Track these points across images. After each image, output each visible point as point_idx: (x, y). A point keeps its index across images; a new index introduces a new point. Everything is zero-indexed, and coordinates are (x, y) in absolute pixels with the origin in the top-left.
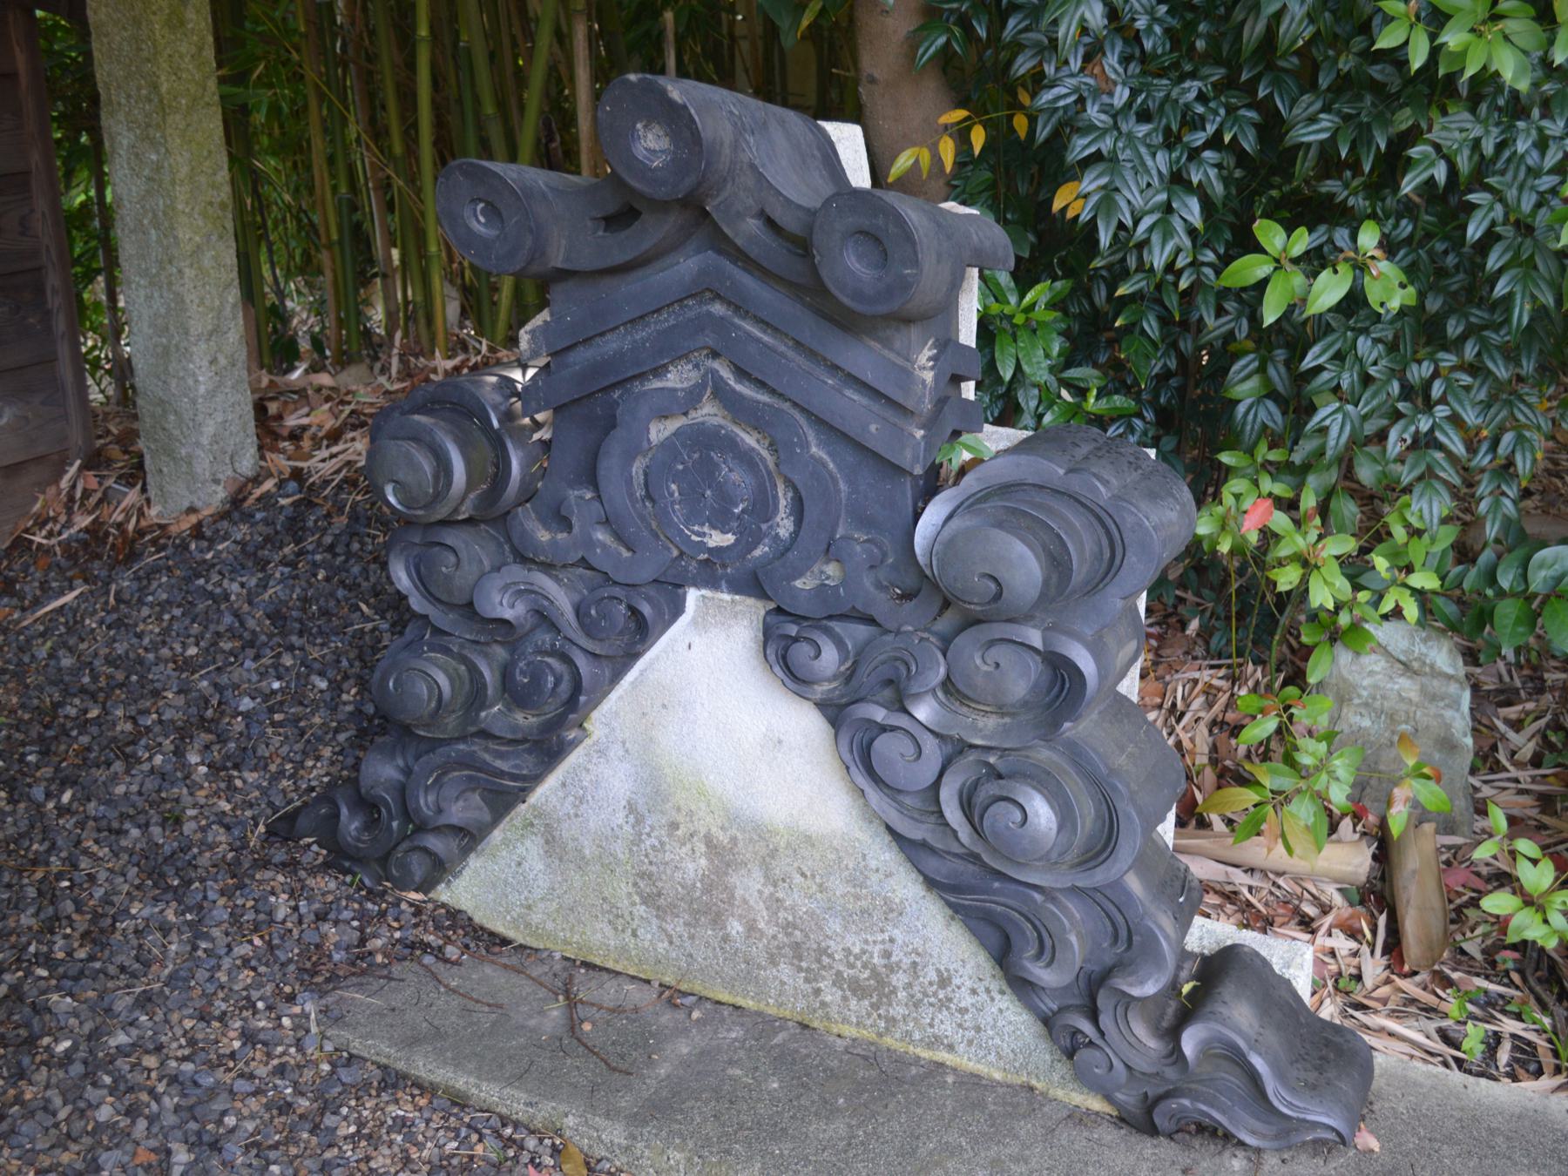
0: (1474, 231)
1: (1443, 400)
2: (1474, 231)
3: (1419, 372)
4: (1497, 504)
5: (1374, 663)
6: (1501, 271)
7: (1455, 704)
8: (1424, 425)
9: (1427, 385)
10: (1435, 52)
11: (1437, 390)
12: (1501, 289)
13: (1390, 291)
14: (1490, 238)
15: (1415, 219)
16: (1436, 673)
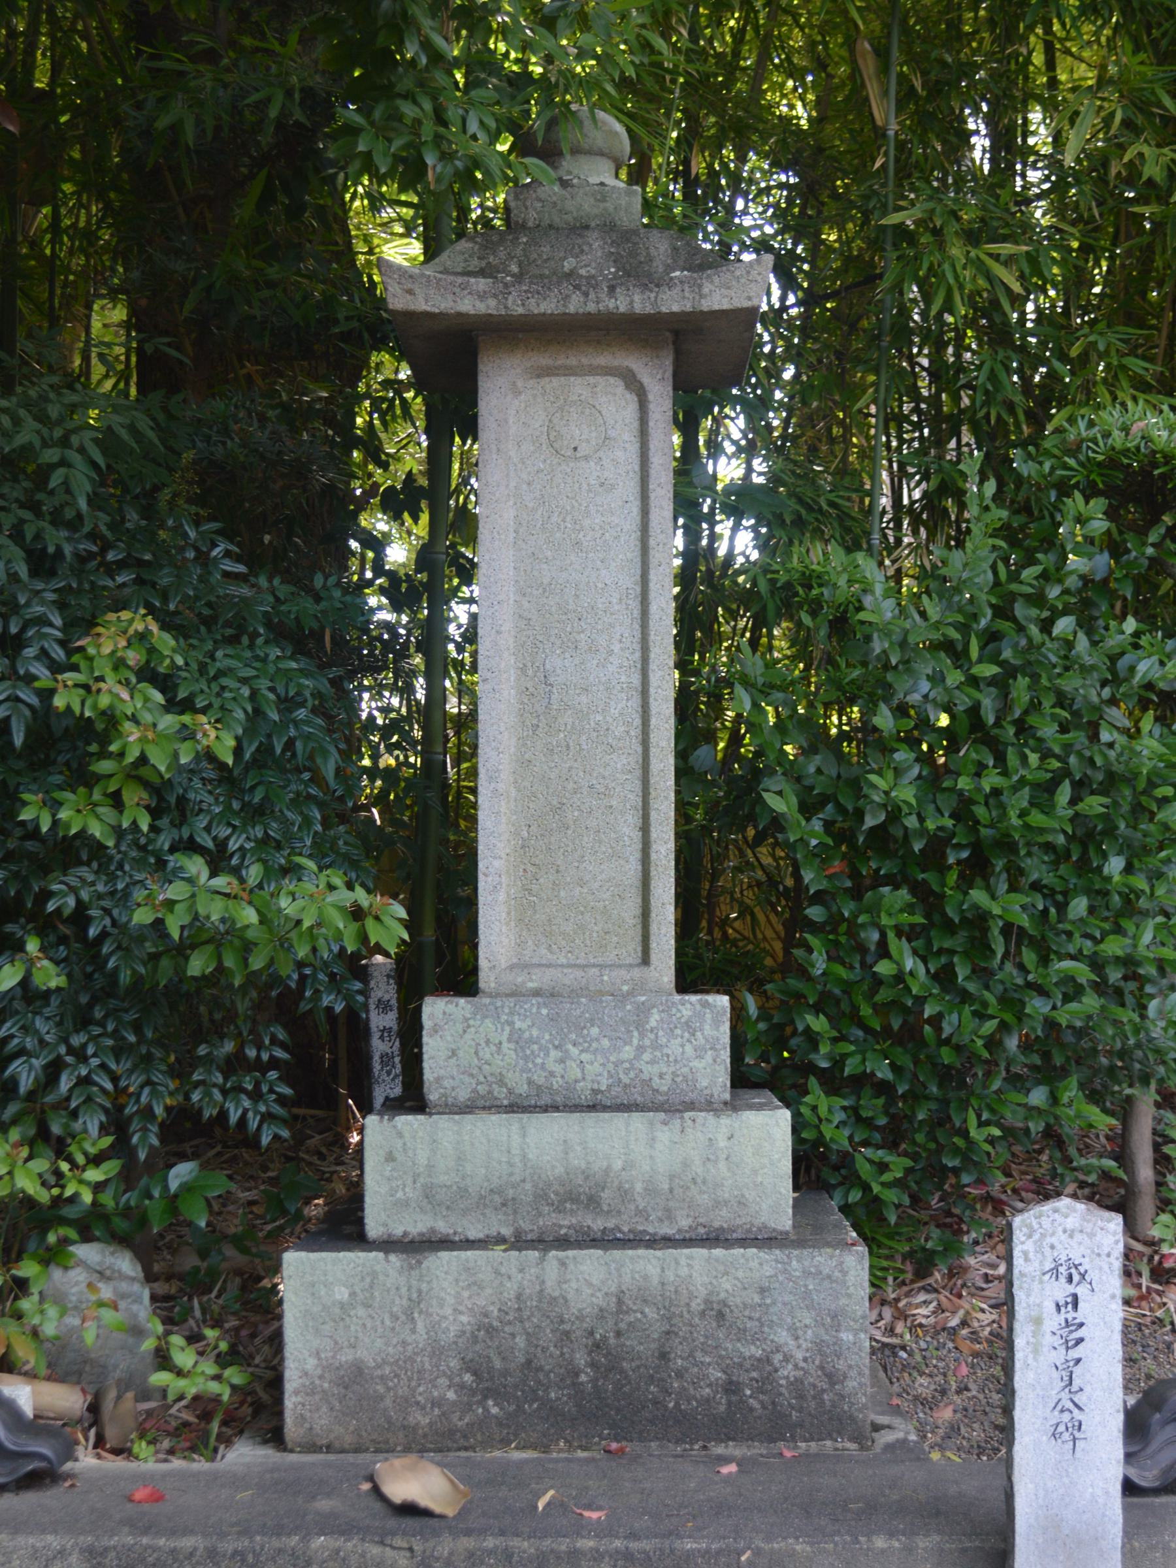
0: (92, 932)
1: (95, 1055)
2: (92, 932)
3: (77, 1040)
4: (144, 1139)
5: (78, 1276)
6: (111, 954)
7: (138, 1300)
8: (84, 1072)
9: (84, 1046)
10: (55, 823)
11: (90, 1050)
12: (111, 964)
13: (49, 976)
14: (104, 935)
15: (68, 947)
16: (122, 1277)
